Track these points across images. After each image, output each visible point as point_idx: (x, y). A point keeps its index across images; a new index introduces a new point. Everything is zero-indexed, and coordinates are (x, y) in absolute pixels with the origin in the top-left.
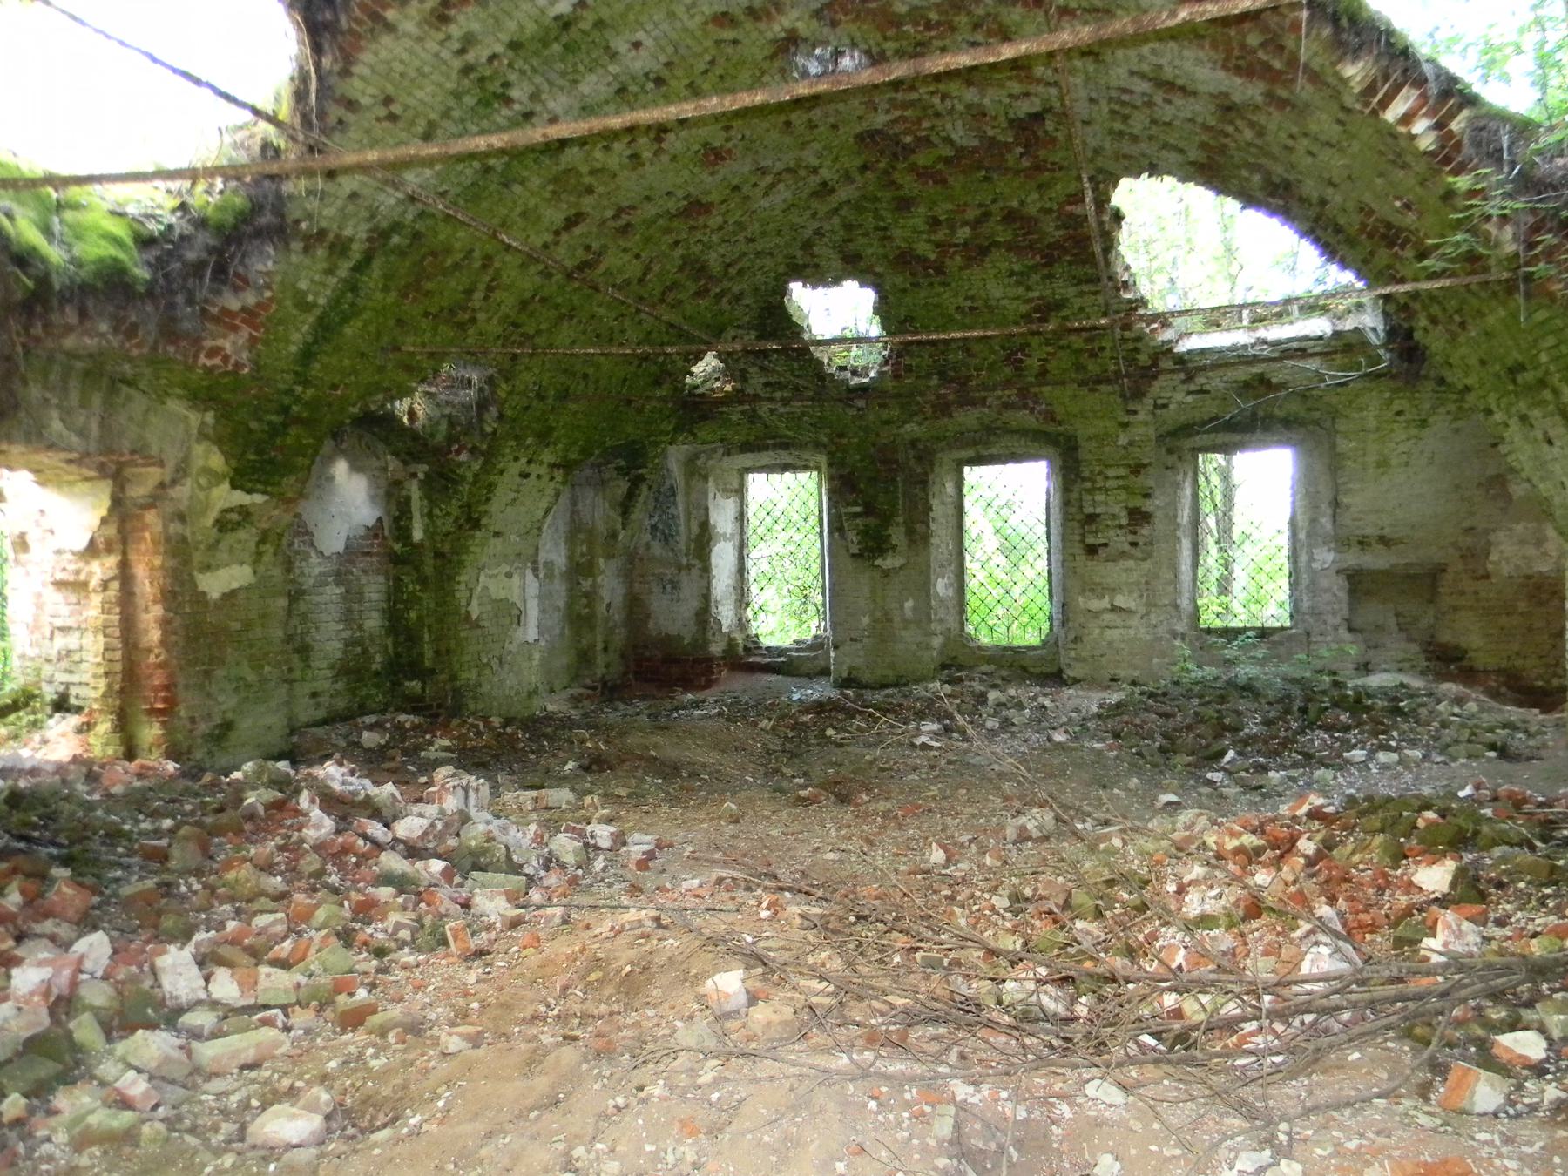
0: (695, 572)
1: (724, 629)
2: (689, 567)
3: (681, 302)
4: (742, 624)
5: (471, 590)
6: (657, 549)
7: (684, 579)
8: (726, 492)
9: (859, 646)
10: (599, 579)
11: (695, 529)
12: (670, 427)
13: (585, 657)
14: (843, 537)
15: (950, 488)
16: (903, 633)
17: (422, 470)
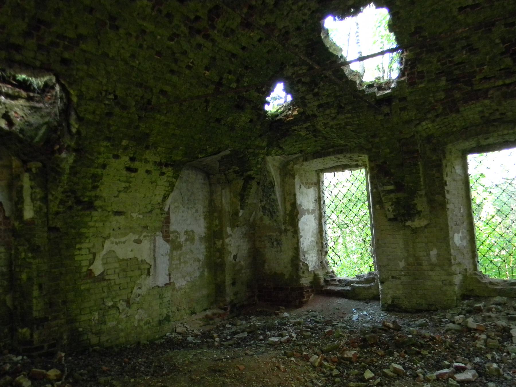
0: (290, 234)
1: (310, 269)
2: (286, 231)
3: (233, 31)
4: (323, 265)
5: (94, 254)
6: (267, 221)
7: (284, 238)
8: (308, 185)
9: (398, 282)
10: (227, 241)
11: (289, 208)
12: (264, 144)
13: (219, 289)
14: (382, 207)
15: (458, 170)
16: (431, 273)
17: (35, 166)
